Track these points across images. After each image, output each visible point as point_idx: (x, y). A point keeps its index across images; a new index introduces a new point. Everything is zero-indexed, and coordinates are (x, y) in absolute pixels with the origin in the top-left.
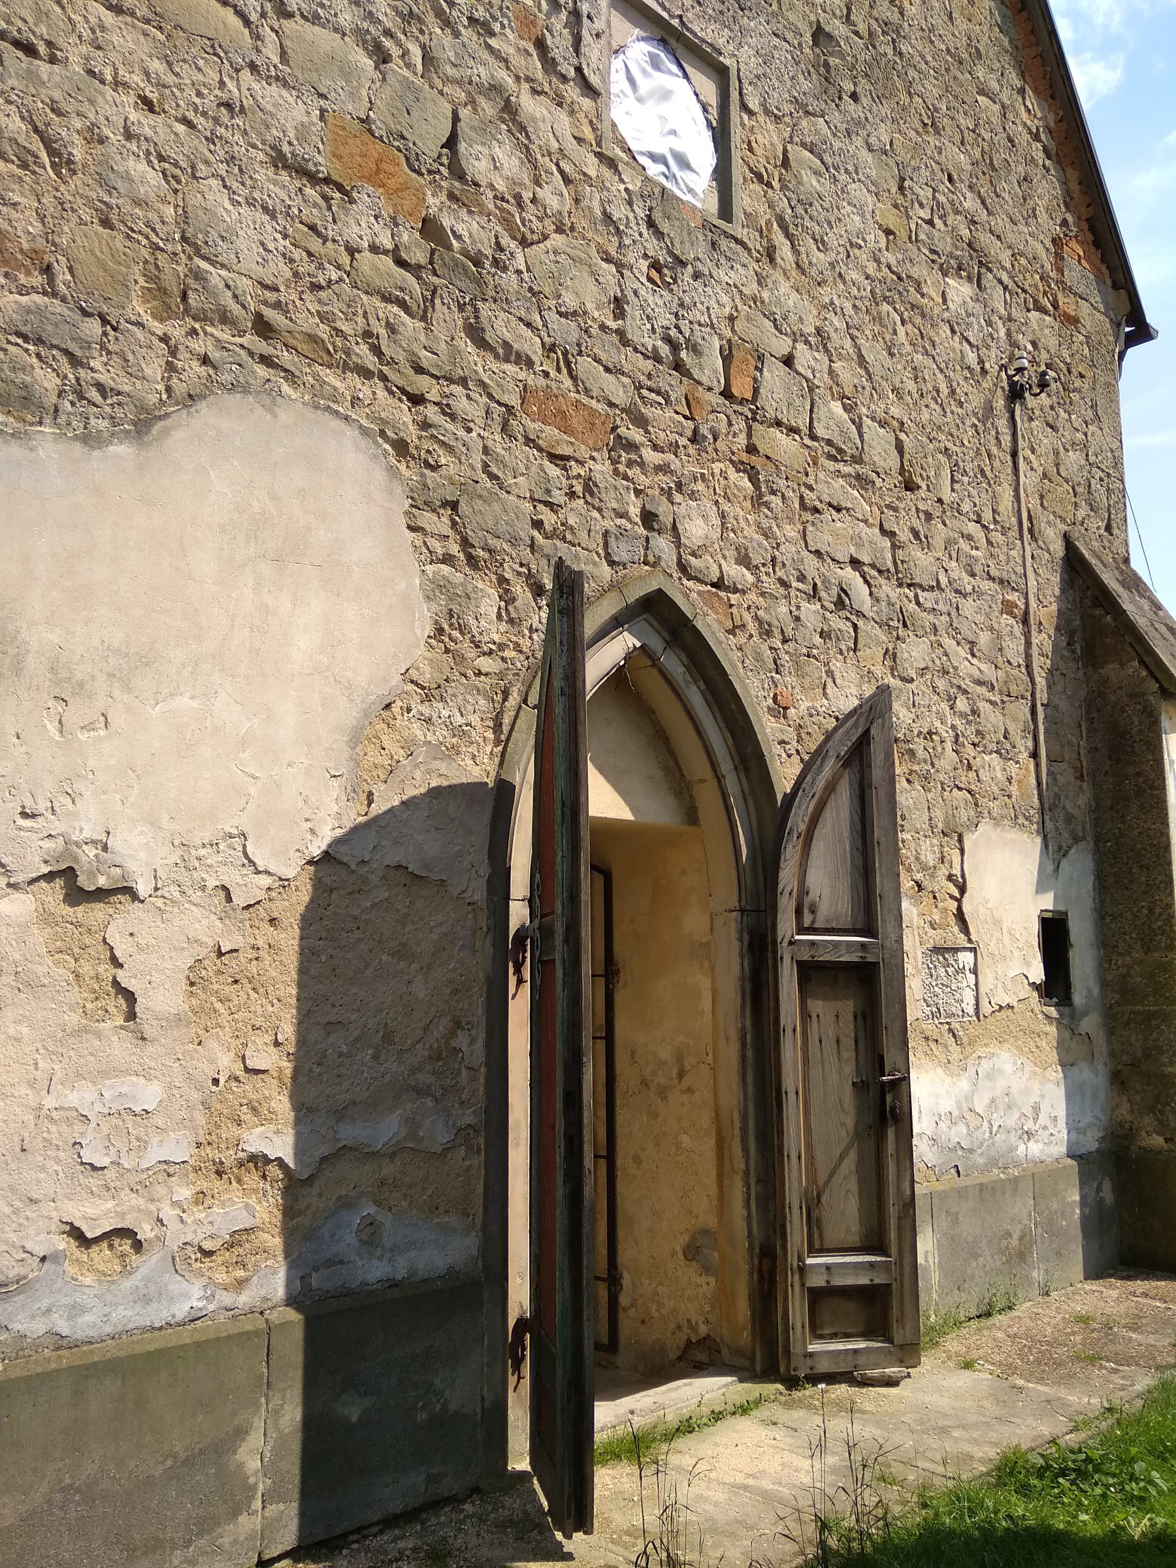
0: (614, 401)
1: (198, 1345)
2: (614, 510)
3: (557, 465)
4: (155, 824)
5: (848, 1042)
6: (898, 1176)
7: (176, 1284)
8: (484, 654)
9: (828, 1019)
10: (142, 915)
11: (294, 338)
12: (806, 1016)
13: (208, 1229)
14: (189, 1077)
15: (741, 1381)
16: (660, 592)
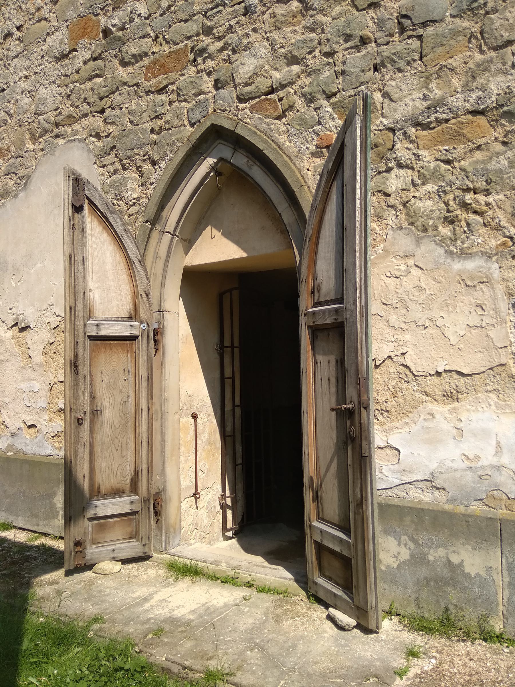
0: (189, 35)
1: (45, 463)
2: (193, 94)
3: (163, 94)
4: (33, 306)
5: (333, 380)
6: (354, 482)
7: (46, 444)
8: (132, 206)
9: (325, 364)
10: (33, 333)
11: (64, 121)
12: (315, 362)
13: (52, 429)
14: (45, 382)
15: (296, 581)
16: (213, 126)
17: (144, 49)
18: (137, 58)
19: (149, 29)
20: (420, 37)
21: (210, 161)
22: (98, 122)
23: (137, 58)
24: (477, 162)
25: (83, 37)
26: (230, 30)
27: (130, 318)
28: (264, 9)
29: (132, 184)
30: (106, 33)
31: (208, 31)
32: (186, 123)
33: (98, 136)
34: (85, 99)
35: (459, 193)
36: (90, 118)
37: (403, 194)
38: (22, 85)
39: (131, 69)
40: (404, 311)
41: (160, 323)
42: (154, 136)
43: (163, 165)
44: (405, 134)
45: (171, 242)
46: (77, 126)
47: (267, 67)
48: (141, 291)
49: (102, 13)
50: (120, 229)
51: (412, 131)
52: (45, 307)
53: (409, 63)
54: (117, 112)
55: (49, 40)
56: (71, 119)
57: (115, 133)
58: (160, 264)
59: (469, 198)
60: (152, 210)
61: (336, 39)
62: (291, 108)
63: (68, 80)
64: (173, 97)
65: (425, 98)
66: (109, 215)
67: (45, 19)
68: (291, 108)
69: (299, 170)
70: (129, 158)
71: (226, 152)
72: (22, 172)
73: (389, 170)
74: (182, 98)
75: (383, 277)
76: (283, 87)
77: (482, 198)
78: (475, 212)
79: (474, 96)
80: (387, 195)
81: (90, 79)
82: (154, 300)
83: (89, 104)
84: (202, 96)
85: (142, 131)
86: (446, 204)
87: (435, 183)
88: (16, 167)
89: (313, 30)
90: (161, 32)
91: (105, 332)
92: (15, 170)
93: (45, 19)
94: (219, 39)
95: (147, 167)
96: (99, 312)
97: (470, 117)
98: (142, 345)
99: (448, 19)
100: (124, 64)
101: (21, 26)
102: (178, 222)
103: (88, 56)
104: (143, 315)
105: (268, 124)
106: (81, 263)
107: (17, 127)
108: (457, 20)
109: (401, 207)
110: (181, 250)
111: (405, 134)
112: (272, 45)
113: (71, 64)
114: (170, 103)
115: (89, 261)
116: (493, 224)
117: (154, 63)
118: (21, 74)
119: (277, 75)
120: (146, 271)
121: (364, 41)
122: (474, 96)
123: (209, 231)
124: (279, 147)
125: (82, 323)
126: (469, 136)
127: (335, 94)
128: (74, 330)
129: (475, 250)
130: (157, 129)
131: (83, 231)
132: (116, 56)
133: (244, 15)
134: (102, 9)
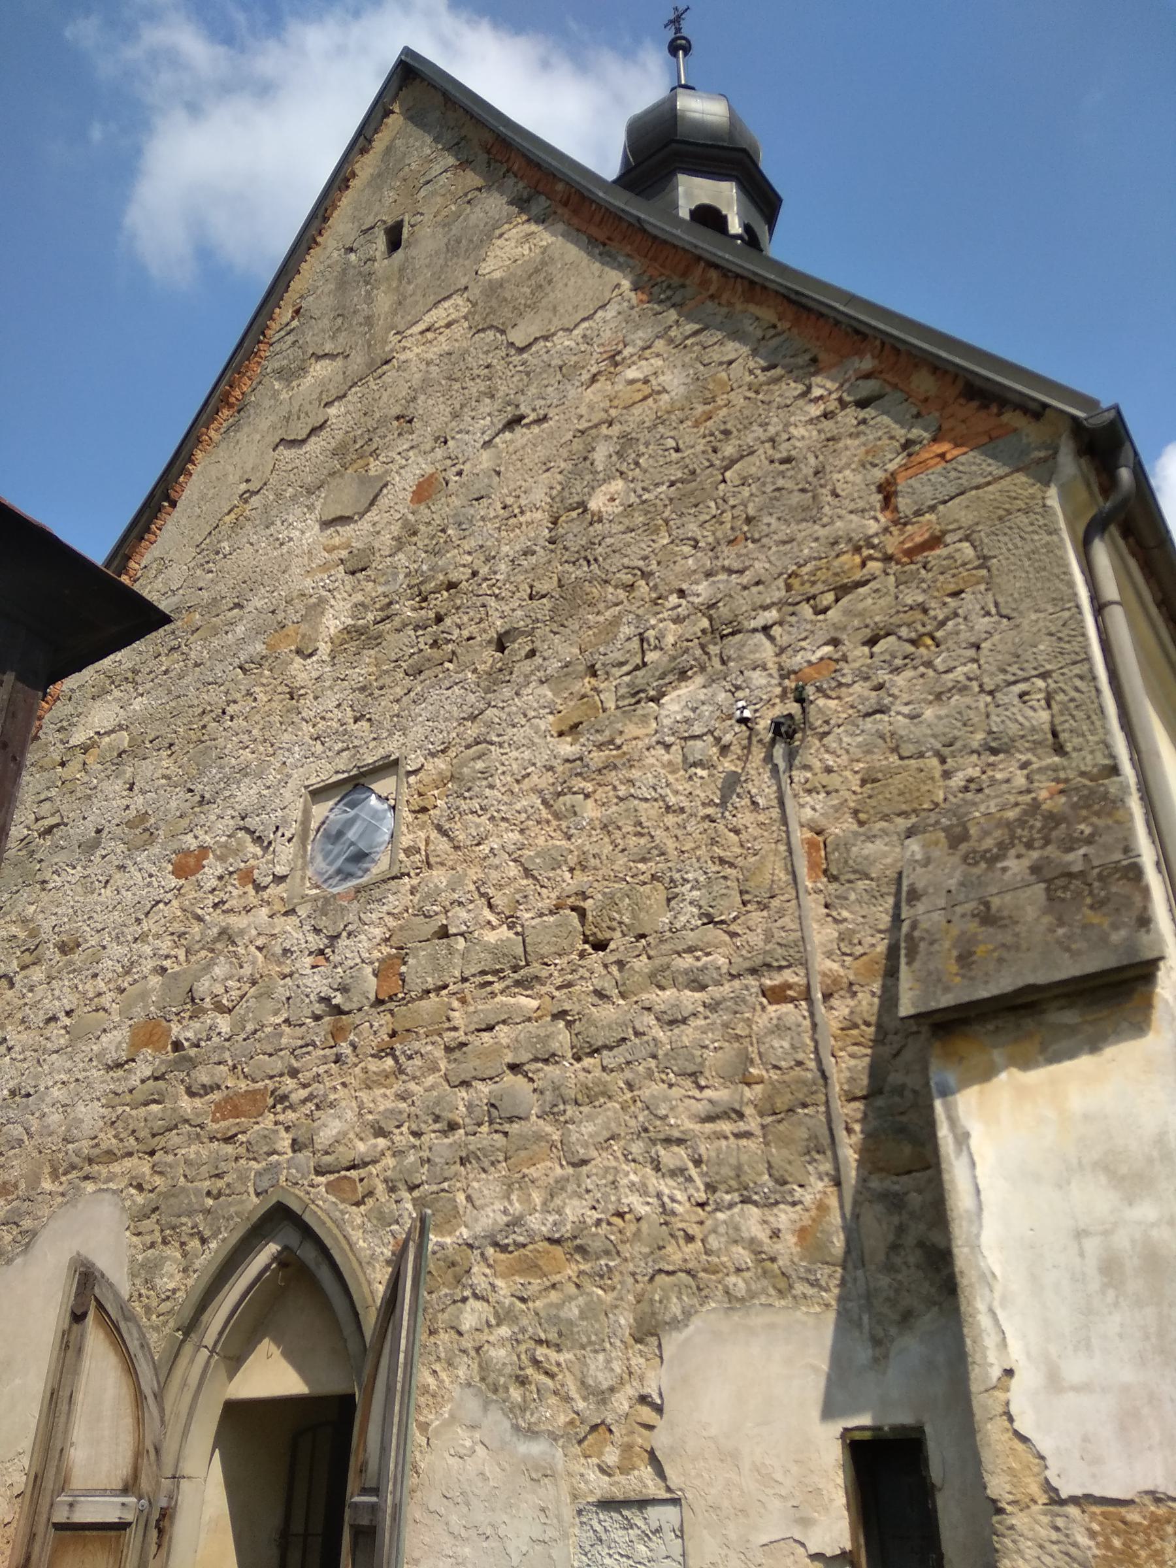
17: (216, 1080)
18: (208, 1089)
19: (227, 1055)
20: (506, 1134)
21: (273, 1248)
22: (144, 1167)
23: (208, 1089)
24: (551, 1305)
25: (146, 1045)
26: (317, 1078)
27: (125, 1491)
28: (355, 1060)
29: (169, 1267)
30: (177, 1046)
31: (294, 1073)
32: (251, 1190)
33: (140, 1187)
34: (134, 1131)
35: (532, 1344)
36: (134, 1160)
37: (477, 1334)
38: (56, 1093)
39: (198, 1103)
40: (465, 1509)
41: (171, 1498)
42: (210, 1202)
43: (213, 1245)
44: (482, 1254)
45: (208, 1363)
46: (116, 1168)
47: (352, 1135)
48: (149, 1445)
49: (175, 1018)
50: (133, 1345)
51: (490, 1251)
52: (11, 1456)
53: (493, 1164)
54: (170, 1158)
55: (104, 1038)
56: (110, 1156)
57: (162, 1189)
58: (187, 1397)
59: (541, 1352)
60: (188, 1313)
61: (425, 1118)
62: (370, 1194)
63: (117, 1100)
64: (242, 1150)
65: (505, 1212)
66: (123, 1326)
67: (105, 1010)
68: (370, 1194)
69: (369, 1283)
70: (173, 1228)
71: (293, 1237)
72: (27, 1223)
73: (464, 1300)
74: (251, 1155)
75: (446, 1455)
76: (366, 1164)
77: (553, 1355)
78: (546, 1373)
79: (551, 1219)
80: (460, 1334)
81: (146, 1104)
82: (168, 1459)
83: (137, 1139)
84: (276, 1157)
85: (197, 1192)
86: (518, 1356)
87: (510, 1326)
88: (20, 1215)
89: (404, 1099)
90: (240, 1063)
91: (80, 1517)
92: (16, 1219)
93: (105, 1010)
94: (305, 1086)
95: (195, 1243)
96: (78, 1482)
97: (546, 1244)
98: (133, 1538)
99: (534, 1118)
100: (191, 1094)
101: (72, 1011)
102: (221, 1334)
103: (148, 1073)
104: (145, 1484)
105: (343, 1213)
106: (66, 1400)
107: (35, 1154)
108: (541, 1122)
109: (473, 1353)
110: (222, 1373)
111: (482, 1254)
112: (360, 1107)
113: (126, 1079)
114: (237, 1159)
115: (80, 1397)
116: (562, 1393)
117: (227, 1099)
118: (57, 1078)
119: (362, 1147)
120: (162, 1411)
121: (452, 1127)
122: (551, 1219)
123: (267, 1346)
124: (351, 1246)
125: (48, 1499)
126: (545, 1269)
127: (418, 1186)
128: (34, 1513)
129: (543, 1427)
130: (215, 1192)
131: (80, 1350)
132: (182, 1081)
133: (336, 1062)
134: (177, 1014)
